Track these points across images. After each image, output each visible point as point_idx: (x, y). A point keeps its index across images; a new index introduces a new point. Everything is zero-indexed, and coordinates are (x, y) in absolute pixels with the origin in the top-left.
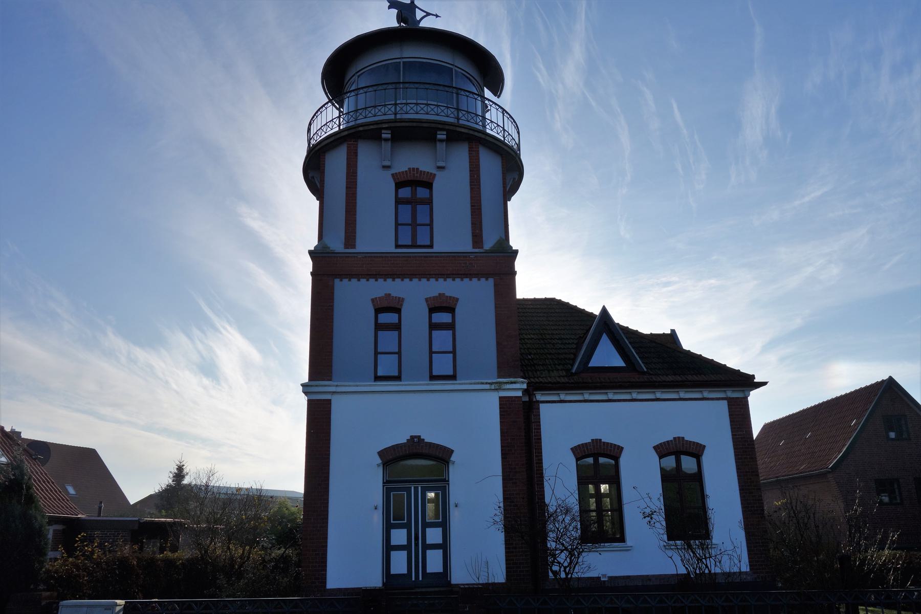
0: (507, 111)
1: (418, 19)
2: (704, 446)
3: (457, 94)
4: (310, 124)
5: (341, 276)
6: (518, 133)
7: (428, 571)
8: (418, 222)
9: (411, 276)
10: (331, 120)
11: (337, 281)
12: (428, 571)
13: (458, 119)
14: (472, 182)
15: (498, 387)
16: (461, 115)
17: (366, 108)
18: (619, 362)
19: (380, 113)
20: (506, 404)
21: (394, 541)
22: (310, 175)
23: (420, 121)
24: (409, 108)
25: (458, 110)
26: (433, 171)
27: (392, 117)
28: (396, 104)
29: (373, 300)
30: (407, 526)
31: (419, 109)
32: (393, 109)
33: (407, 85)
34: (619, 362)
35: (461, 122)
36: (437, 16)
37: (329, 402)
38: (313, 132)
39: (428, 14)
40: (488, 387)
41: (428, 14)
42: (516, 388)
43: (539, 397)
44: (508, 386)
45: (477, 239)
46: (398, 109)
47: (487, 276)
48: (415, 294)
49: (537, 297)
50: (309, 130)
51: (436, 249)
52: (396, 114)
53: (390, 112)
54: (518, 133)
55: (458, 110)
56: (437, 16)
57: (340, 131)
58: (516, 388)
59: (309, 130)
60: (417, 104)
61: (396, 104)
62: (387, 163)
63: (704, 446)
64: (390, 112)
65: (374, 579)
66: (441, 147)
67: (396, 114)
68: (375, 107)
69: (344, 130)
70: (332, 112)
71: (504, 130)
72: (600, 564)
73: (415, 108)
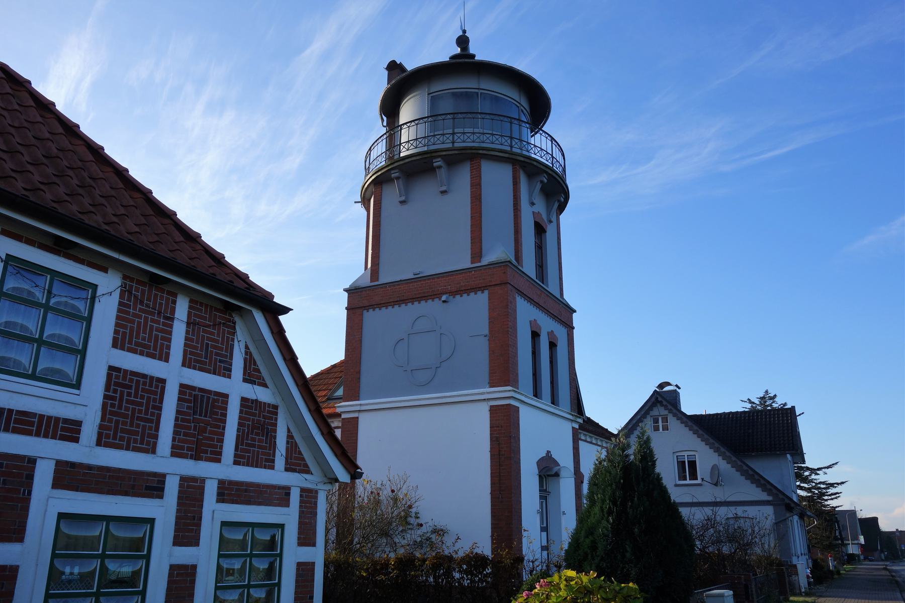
0: (568, 137)
3: (511, 123)
7: (309, 372)
12: (309, 372)
13: (511, 147)
19: (469, 140)
24: (485, 138)
25: (511, 138)
27: (450, 145)
28: (453, 134)
32: (451, 138)
35: (514, 150)
37: (356, 419)
46: (456, 138)
47: (482, 289)
52: (453, 143)
53: (448, 141)
55: (511, 138)
60: (443, 135)
61: (453, 134)
62: (444, 188)
64: (448, 141)
66: (442, 173)
67: (453, 143)
71: (553, 157)
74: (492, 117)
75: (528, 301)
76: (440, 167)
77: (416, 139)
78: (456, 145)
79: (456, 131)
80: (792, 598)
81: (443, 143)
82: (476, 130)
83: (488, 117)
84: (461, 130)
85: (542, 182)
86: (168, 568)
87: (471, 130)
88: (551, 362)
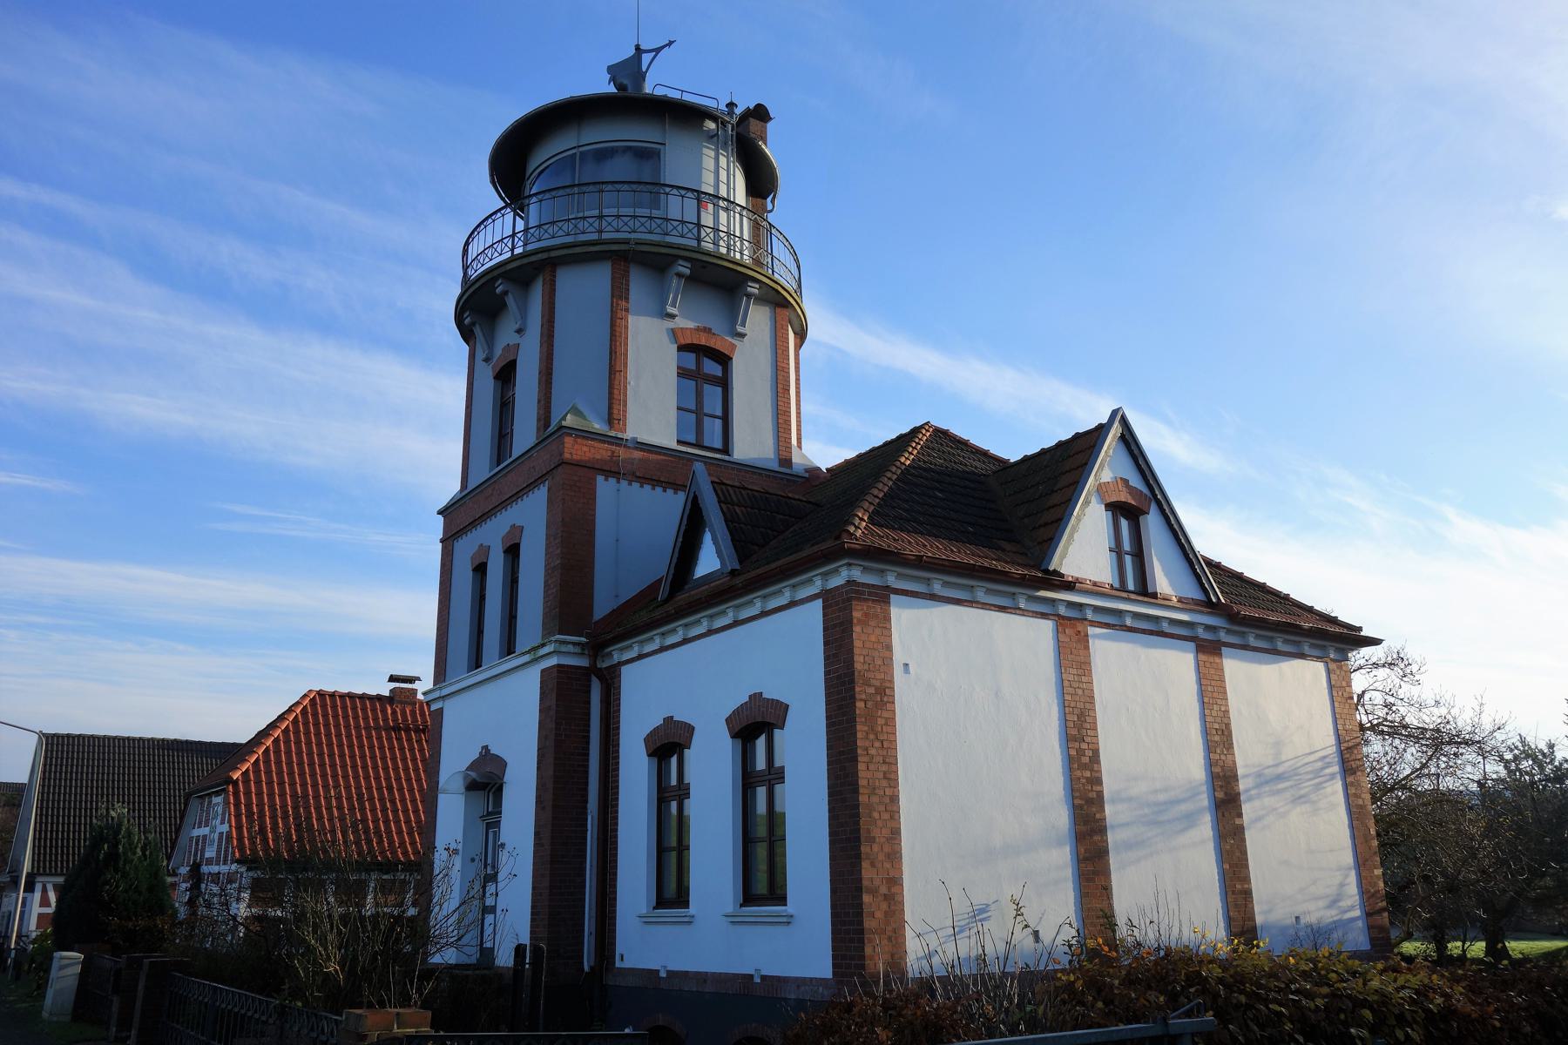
4: (467, 244)
6: (797, 261)
8: (706, 410)
10: (504, 237)
16: (703, 234)
17: (553, 223)
18: (540, 496)
22: (467, 321)
23: (626, 242)
27: (595, 237)
28: (601, 217)
31: (638, 224)
32: (596, 224)
33: (584, 189)
34: (540, 496)
38: (474, 250)
50: (465, 251)
54: (797, 261)
57: (513, 258)
59: (465, 251)
60: (618, 216)
61: (601, 217)
67: (600, 232)
68: (553, 223)
69: (521, 256)
70: (507, 223)
73: (631, 223)
74: (634, 187)
75: (505, 508)
76: (505, 293)
77: (539, 226)
78: (605, 236)
79: (606, 212)
80: (583, 639)
81: (559, 237)
82: (639, 212)
83: (626, 187)
84: (614, 211)
85: (679, 275)
86: (474, 754)
87: (646, 212)
88: (482, 598)
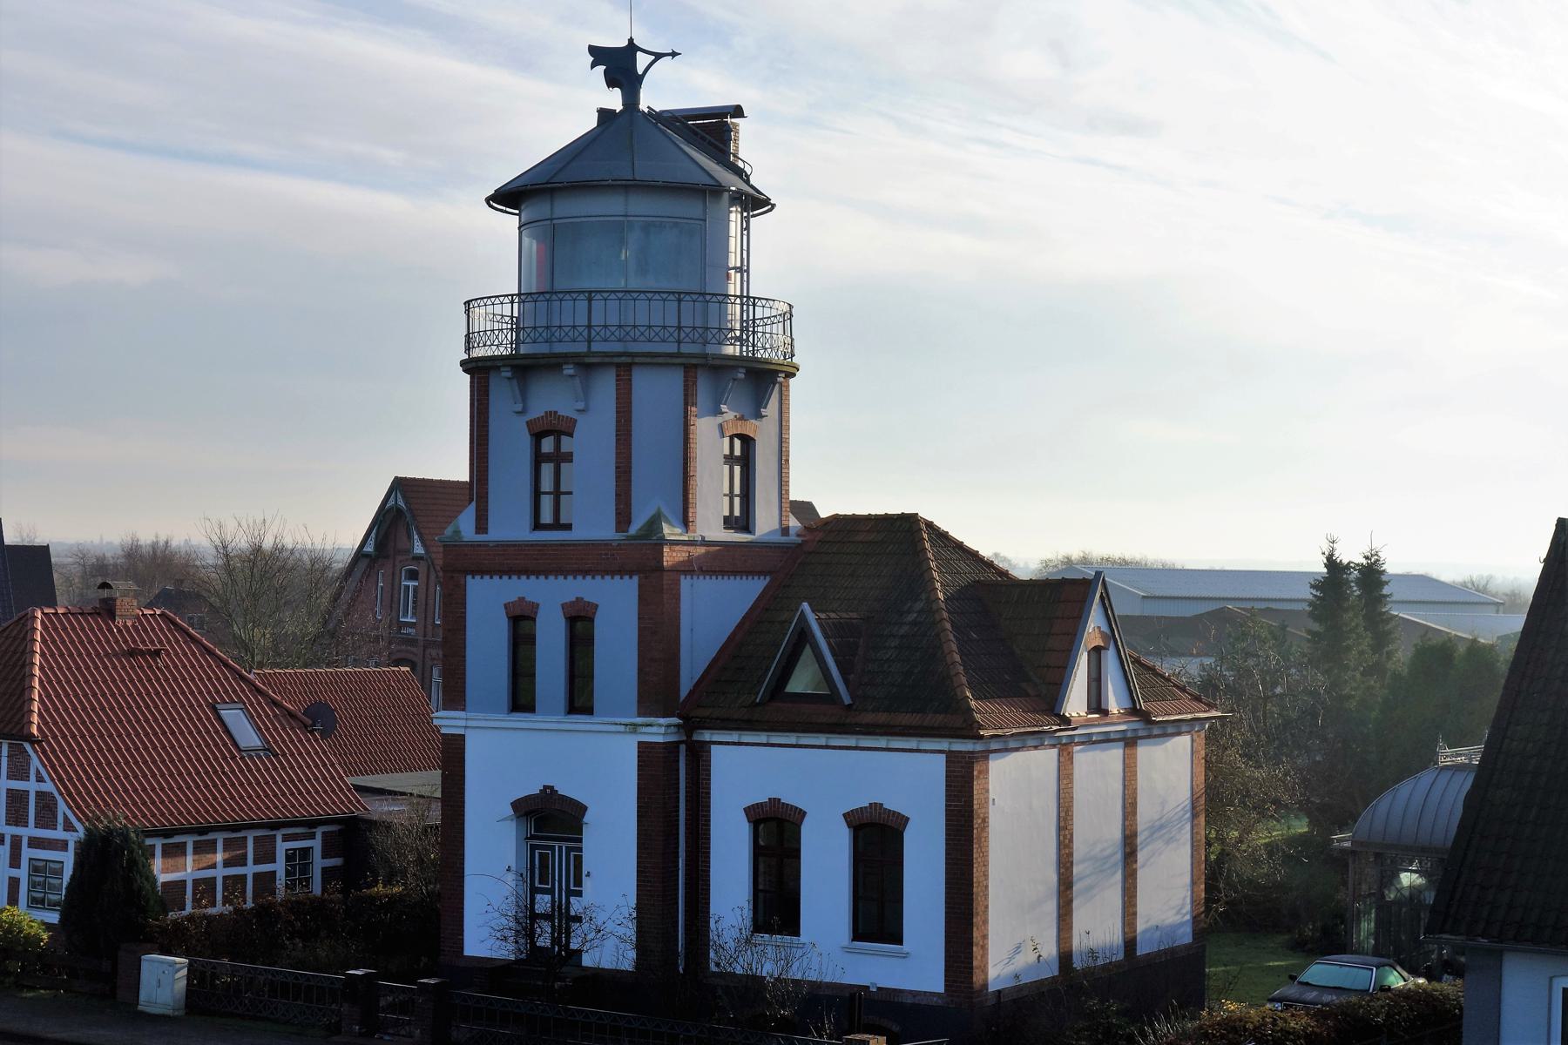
1: (640, 72)
2: (908, 819)
5: (474, 573)
9: (545, 572)
11: (469, 578)
14: (629, 421)
15: (634, 728)
20: (644, 749)
21: (539, 909)
26: (574, 416)
29: (506, 606)
30: (551, 892)
36: (674, 54)
39: (658, 56)
40: (622, 728)
41: (658, 56)
42: (659, 731)
43: (707, 736)
44: (644, 729)
45: (623, 517)
47: (631, 574)
48: (550, 596)
49: (858, 513)
51: (578, 534)
56: (674, 54)
58: (659, 731)
63: (908, 819)
65: (504, 951)
72: (767, 960)
